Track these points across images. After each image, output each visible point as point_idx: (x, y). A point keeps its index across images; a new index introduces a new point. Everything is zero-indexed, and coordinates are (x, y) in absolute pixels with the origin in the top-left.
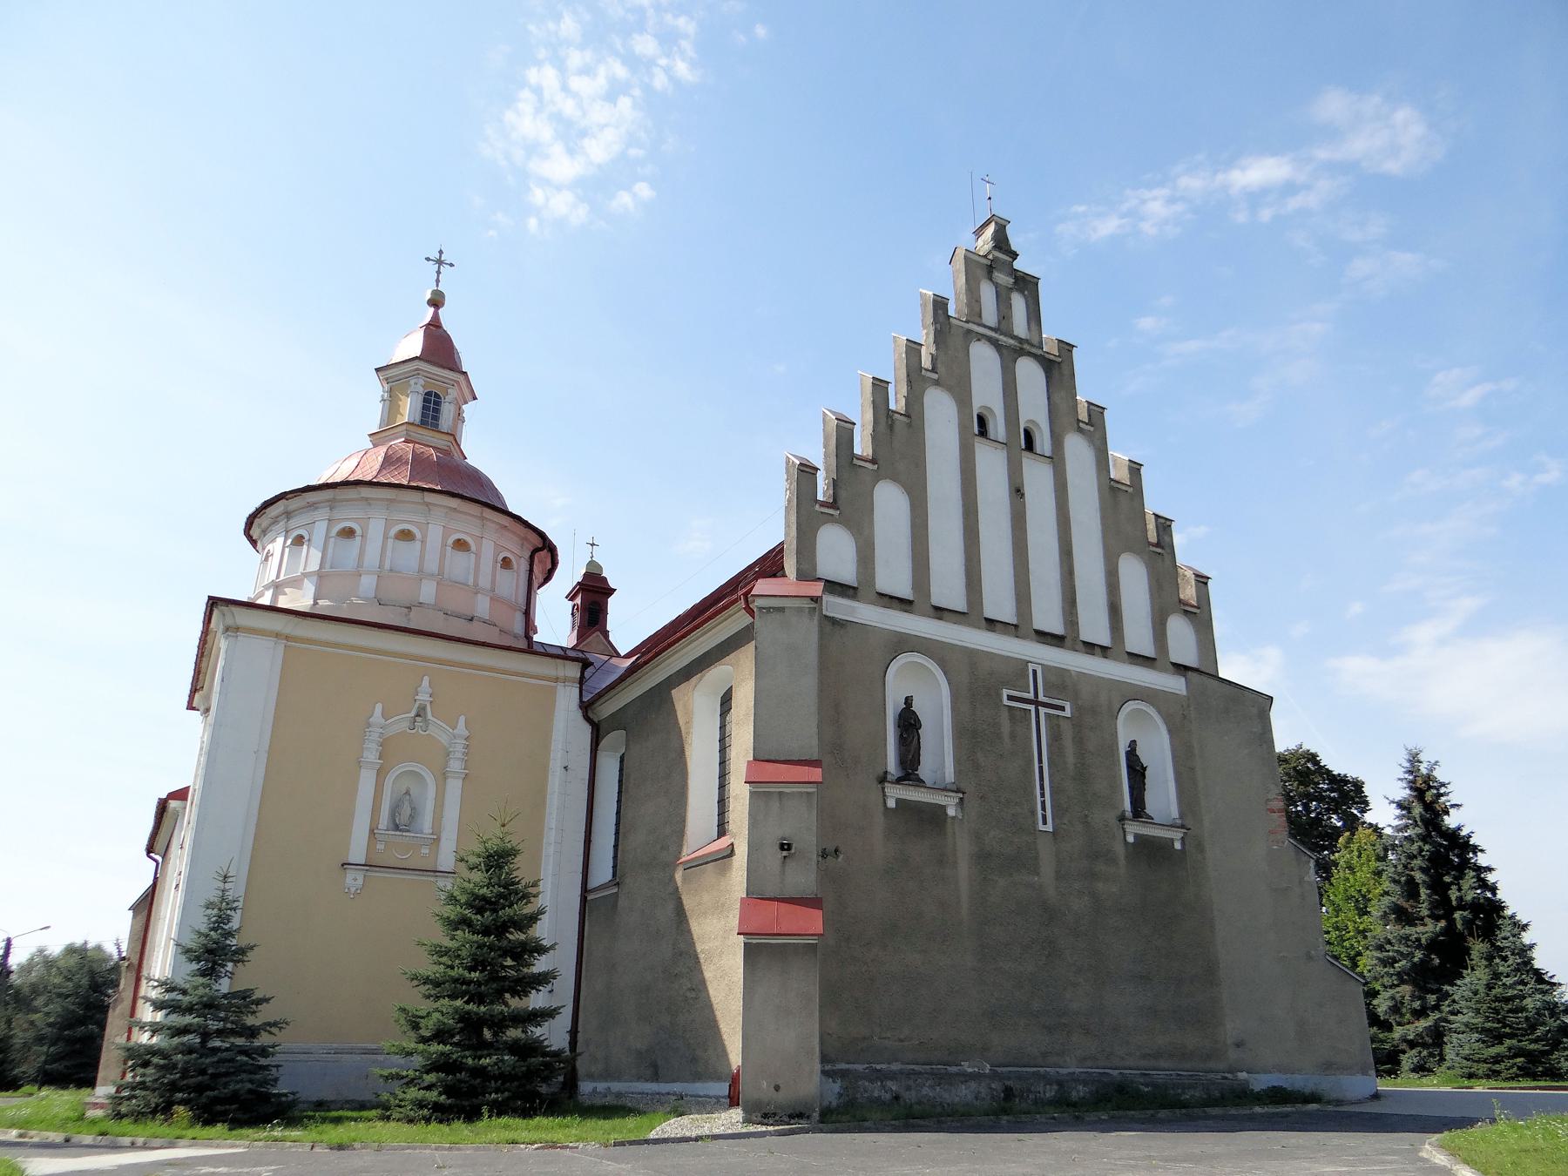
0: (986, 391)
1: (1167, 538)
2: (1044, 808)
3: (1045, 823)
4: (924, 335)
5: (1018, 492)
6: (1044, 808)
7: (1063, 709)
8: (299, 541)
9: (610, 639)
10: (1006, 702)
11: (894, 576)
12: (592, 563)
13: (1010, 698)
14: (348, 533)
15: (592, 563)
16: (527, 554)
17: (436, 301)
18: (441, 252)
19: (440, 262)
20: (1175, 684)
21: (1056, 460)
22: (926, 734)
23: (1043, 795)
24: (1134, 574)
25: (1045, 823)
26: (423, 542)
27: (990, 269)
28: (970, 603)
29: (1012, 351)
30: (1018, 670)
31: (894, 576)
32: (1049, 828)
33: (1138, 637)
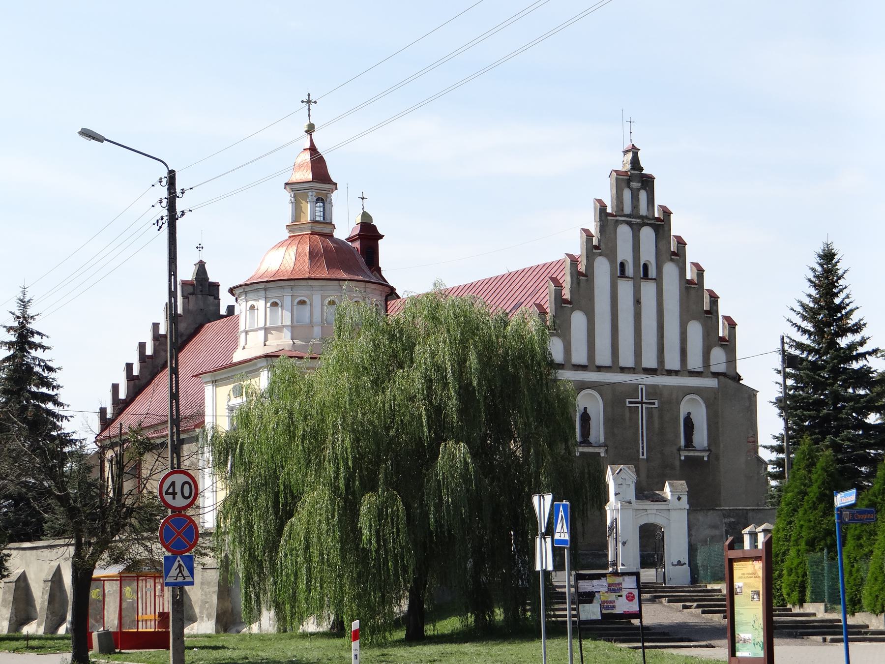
0: (624, 252)
1: (715, 308)
2: (643, 449)
3: (643, 455)
4: (593, 228)
5: (638, 302)
6: (643, 449)
7: (654, 404)
8: (275, 304)
9: (383, 274)
10: (628, 404)
11: (579, 356)
12: (365, 215)
13: (630, 402)
14: (302, 302)
15: (365, 215)
16: (384, 298)
17: (311, 129)
18: (309, 95)
19: (309, 102)
20: (712, 383)
21: (659, 280)
22: (593, 423)
23: (643, 443)
24: (695, 330)
25: (643, 455)
26: (311, 305)
27: (628, 182)
28: (613, 362)
29: (637, 222)
30: (633, 390)
31: (579, 356)
32: (645, 457)
33: (695, 362)
